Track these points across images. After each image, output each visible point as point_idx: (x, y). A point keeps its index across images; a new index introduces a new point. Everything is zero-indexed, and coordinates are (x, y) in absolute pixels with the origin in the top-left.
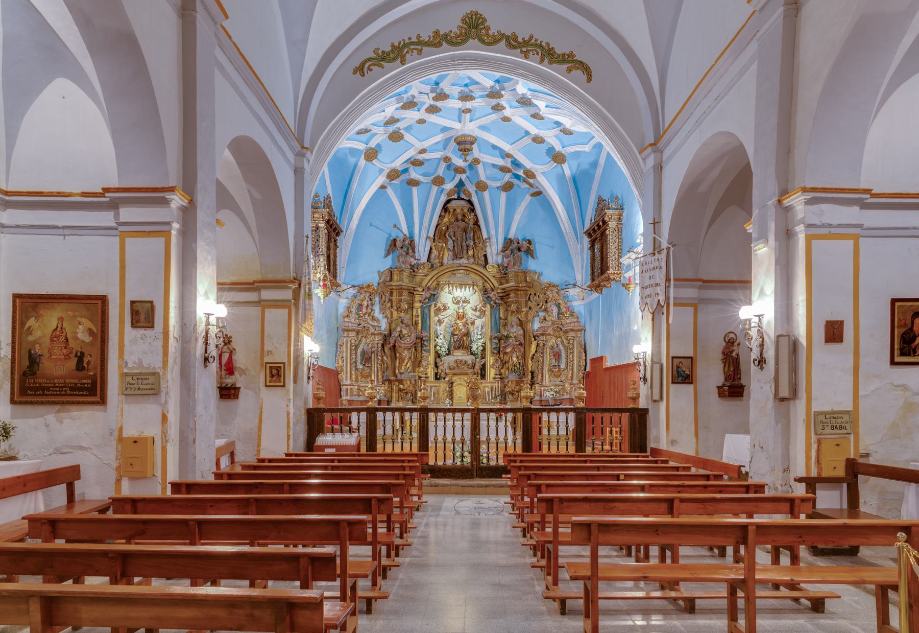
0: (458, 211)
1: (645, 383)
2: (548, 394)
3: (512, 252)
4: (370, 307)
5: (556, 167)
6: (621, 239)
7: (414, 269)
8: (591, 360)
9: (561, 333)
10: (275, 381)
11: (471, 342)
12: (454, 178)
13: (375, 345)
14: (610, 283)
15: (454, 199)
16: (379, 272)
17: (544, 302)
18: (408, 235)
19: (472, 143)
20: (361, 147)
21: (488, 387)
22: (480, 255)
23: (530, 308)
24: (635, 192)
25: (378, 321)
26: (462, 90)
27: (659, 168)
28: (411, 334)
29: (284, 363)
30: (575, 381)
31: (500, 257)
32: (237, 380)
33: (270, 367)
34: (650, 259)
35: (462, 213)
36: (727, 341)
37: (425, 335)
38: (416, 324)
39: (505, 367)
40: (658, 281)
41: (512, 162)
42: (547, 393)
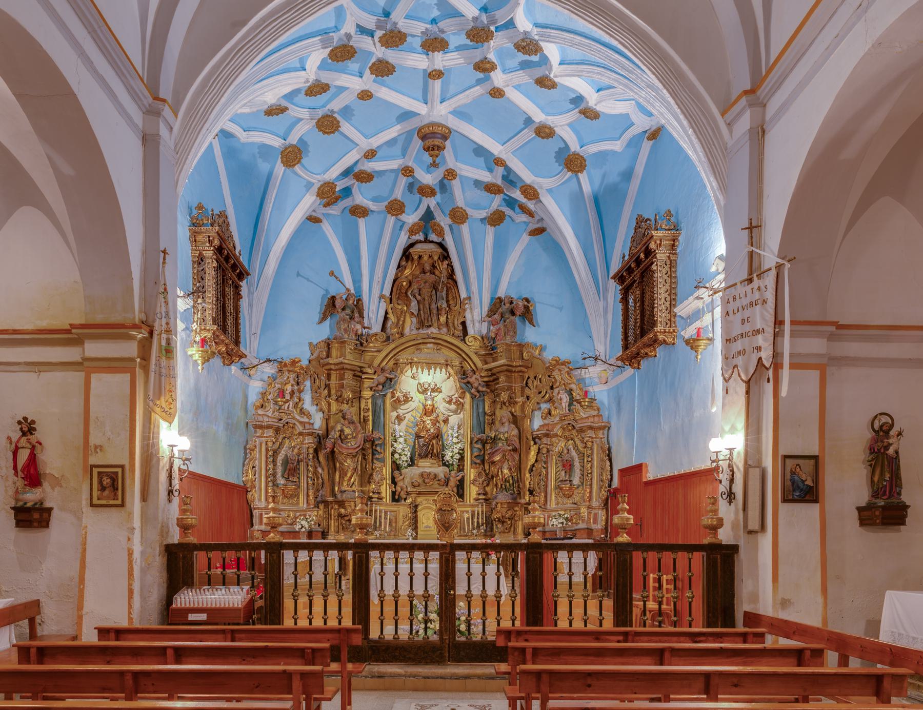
0: (426, 258)
1: (730, 502)
2: (555, 522)
3: (502, 316)
4: (297, 394)
5: (569, 179)
6: (675, 277)
7: (361, 342)
8: (621, 471)
9: (574, 433)
10: (108, 498)
11: (443, 447)
12: (418, 206)
13: (305, 450)
14: (655, 349)
15: (421, 242)
16: (310, 344)
17: (548, 388)
18: (353, 291)
19: (445, 138)
20: (276, 143)
21: (467, 512)
22: (456, 323)
23: (528, 398)
24: (710, 183)
25: (309, 415)
26: (427, 29)
27: (759, 133)
28: (357, 434)
29: (122, 467)
30: (595, 503)
31: (485, 325)
32: (49, 495)
33: (99, 473)
34: (741, 289)
35: (430, 261)
36: (876, 426)
37: (378, 435)
38: (366, 421)
39: (491, 483)
40: (759, 326)
41: (504, 178)
42: (554, 520)
